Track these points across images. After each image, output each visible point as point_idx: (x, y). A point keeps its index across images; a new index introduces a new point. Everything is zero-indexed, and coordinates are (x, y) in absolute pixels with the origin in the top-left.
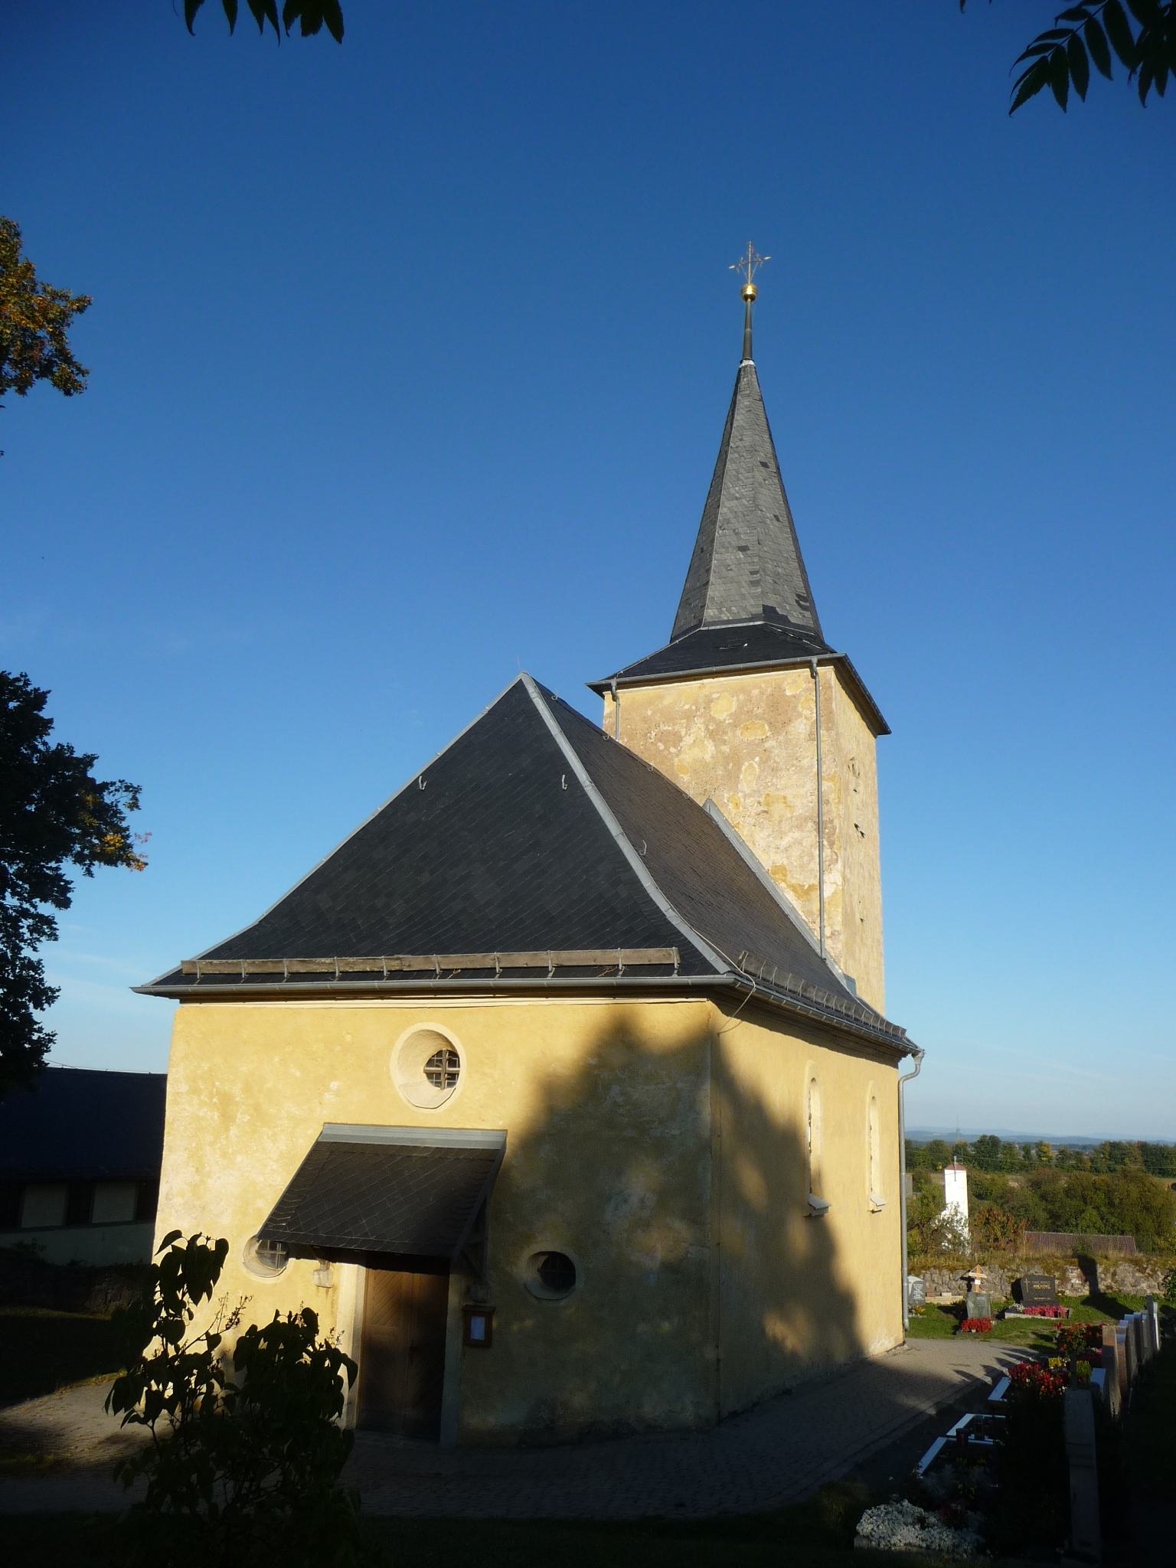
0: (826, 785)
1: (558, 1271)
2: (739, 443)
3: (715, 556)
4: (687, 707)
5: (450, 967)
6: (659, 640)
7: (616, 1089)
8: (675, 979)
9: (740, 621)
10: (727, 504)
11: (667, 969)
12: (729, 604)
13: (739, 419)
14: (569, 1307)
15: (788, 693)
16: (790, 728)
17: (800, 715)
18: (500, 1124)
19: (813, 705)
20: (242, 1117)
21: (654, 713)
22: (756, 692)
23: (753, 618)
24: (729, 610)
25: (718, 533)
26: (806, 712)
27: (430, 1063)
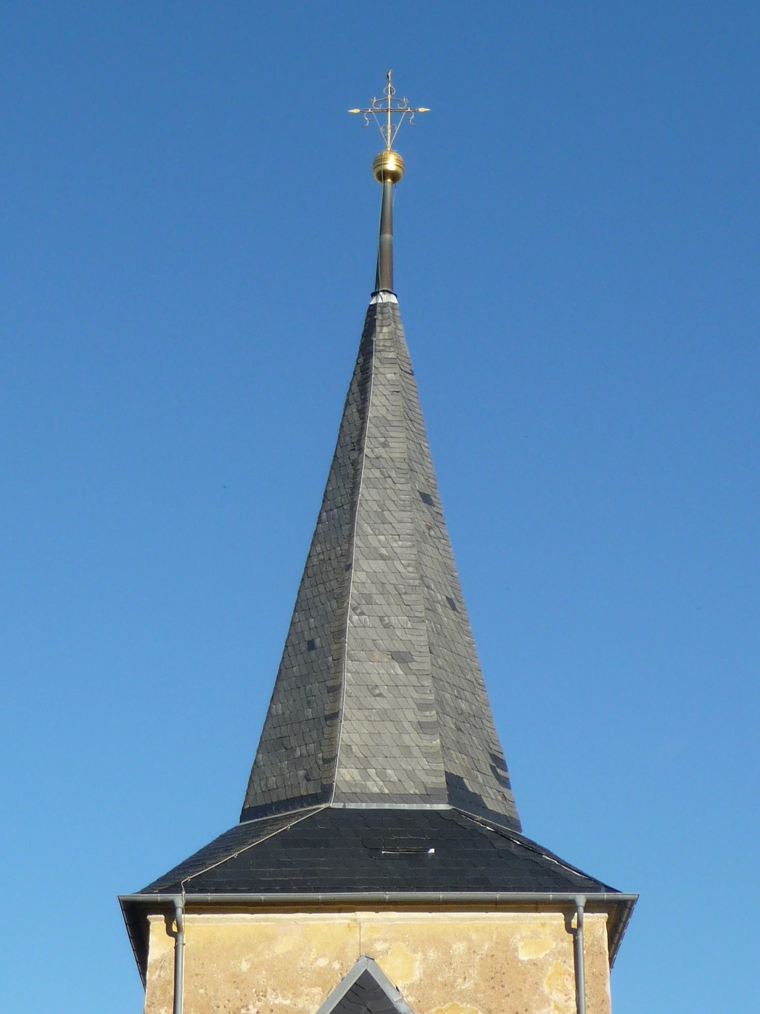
2: (380, 451)
3: (348, 663)
4: (322, 962)
6: (213, 810)
9: (405, 798)
10: (364, 564)
12: (382, 760)
13: (380, 402)
15: (524, 956)
19: (571, 985)
22: (459, 947)
23: (427, 797)
24: (382, 775)
25: (352, 620)
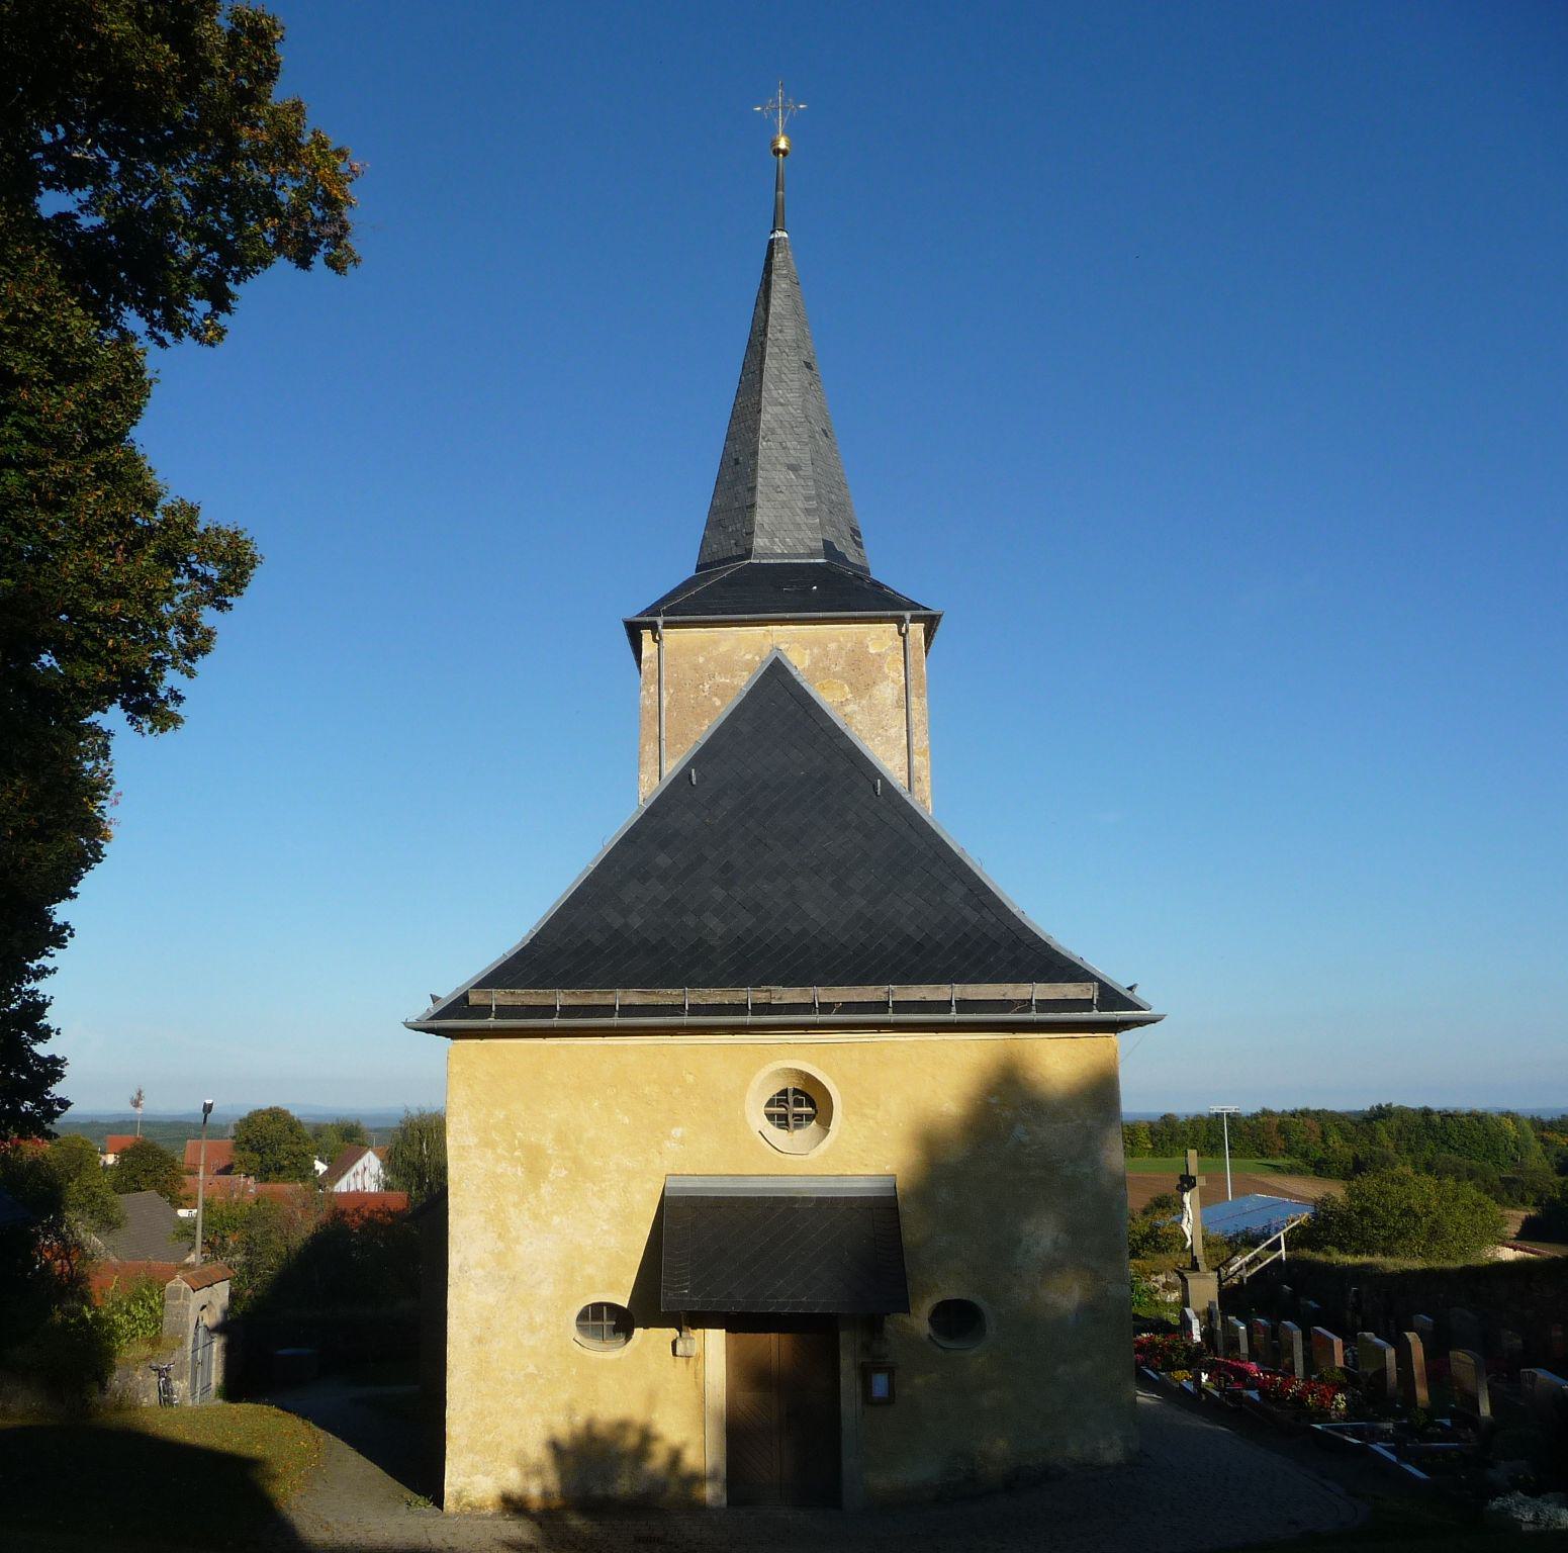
0: (917, 760)
1: (958, 1319)
2: (779, 335)
4: (748, 657)
5: (832, 1000)
7: (1019, 1129)
8: (1096, 1015)
9: (777, 556)
10: (769, 409)
11: (1086, 1005)
12: (782, 532)
13: (777, 303)
14: (975, 1358)
15: (872, 650)
16: (875, 691)
17: (887, 677)
18: (888, 1169)
19: (901, 667)
20: (556, 1172)
21: (707, 661)
22: (833, 646)
23: (811, 555)
24: (784, 543)
25: (763, 445)
26: (893, 674)
27: (770, 1103)
